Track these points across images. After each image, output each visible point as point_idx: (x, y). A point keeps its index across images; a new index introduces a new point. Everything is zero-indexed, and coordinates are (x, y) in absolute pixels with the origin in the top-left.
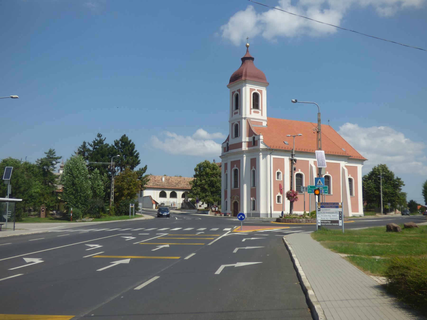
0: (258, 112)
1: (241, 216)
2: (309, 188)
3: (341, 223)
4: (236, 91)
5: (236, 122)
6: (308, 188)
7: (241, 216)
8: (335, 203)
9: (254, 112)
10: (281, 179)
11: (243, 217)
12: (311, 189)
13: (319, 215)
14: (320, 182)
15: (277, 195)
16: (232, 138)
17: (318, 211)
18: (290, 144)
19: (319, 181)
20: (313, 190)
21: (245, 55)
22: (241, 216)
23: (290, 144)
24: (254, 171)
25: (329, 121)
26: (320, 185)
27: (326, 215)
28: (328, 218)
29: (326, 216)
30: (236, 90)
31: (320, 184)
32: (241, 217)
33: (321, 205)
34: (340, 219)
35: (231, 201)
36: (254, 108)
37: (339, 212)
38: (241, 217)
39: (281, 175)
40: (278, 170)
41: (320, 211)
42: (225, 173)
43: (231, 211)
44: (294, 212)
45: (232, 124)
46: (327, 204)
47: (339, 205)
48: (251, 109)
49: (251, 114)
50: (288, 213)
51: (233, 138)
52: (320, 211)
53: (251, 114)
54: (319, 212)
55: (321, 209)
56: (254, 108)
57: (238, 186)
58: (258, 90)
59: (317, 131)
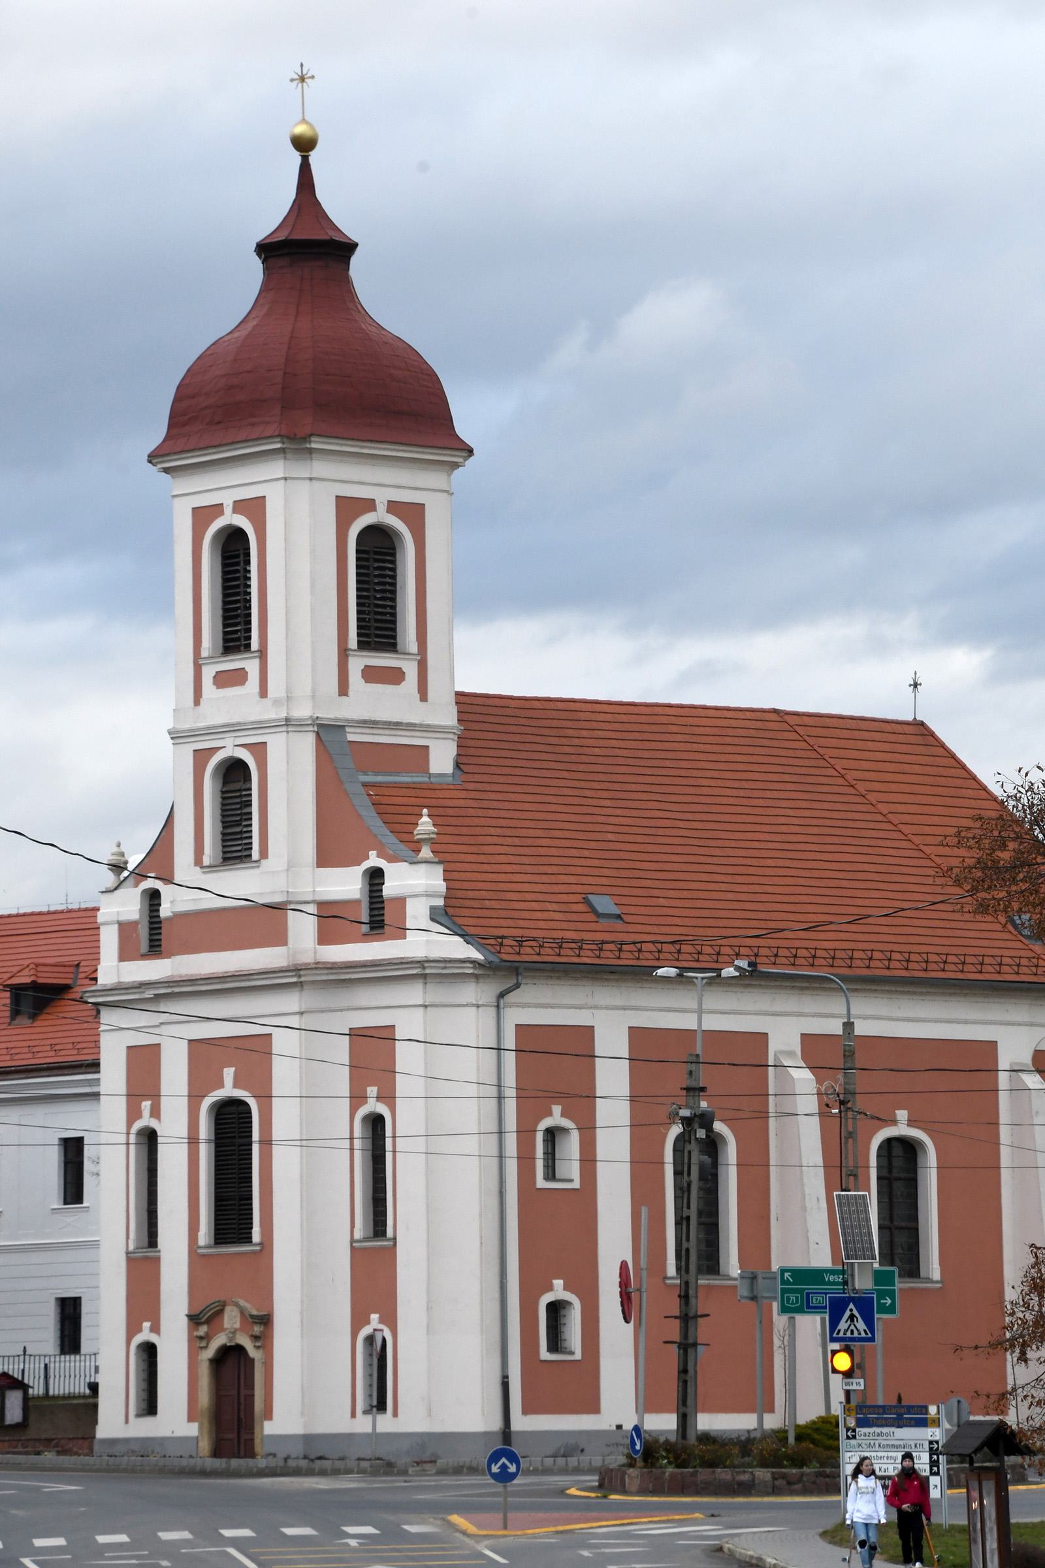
0: (395, 676)
1: (504, 1460)
2: (788, 1282)
3: (936, 1486)
4: (228, 510)
5: (230, 748)
6: (783, 1282)
7: (504, 1464)
8: (913, 1407)
9: (372, 675)
10: (572, 1181)
11: (512, 1469)
12: (800, 1291)
13: (849, 1454)
14: (852, 1318)
15: (547, 1298)
16: (198, 861)
17: (848, 1438)
18: (633, 910)
19: (848, 1313)
20: (808, 1294)
21: (289, 235)
22: (504, 1460)
23: (633, 910)
24: (376, 1123)
25: (915, 685)
26: (852, 1332)
27: (879, 1454)
28: (884, 1466)
29: (879, 1461)
30: (227, 499)
31: (852, 1327)
32: (504, 1467)
33: (857, 1414)
34: (932, 1474)
35: (196, 1343)
36: (367, 643)
37: (931, 1443)
38: (504, 1467)
39: (571, 1146)
40: (550, 1114)
41: (854, 1437)
42: (130, 1124)
43: (191, 1418)
44: (706, 1422)
45: (201, 757)
46: (881, 1411)
47: (927, 1413)
48: (344, 654)
49: (343, 690)
50: (619, 1427)
51: (206, 861)
52: (854, 1437)
53: (343, 690)
54: (853, 1442)
55: (861, 1431)
56: (367, 643)
57: (256, 1236)
58: (394, 507)
59: (842, 1099)
